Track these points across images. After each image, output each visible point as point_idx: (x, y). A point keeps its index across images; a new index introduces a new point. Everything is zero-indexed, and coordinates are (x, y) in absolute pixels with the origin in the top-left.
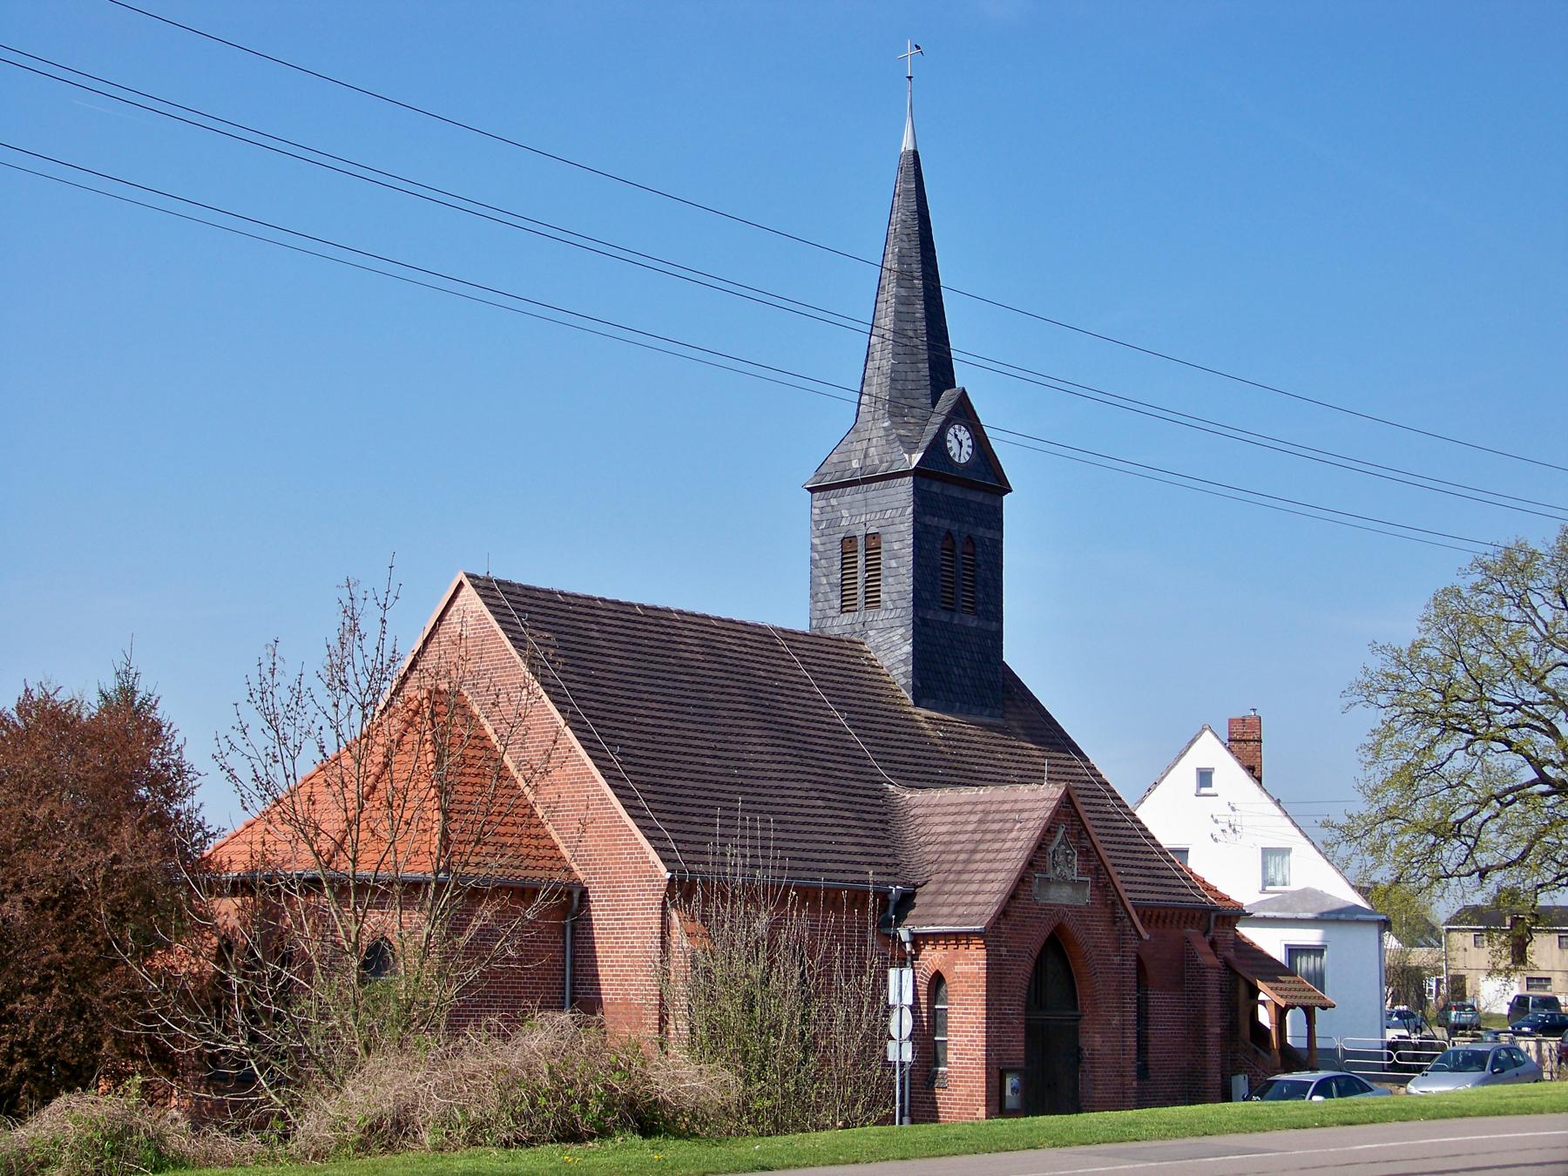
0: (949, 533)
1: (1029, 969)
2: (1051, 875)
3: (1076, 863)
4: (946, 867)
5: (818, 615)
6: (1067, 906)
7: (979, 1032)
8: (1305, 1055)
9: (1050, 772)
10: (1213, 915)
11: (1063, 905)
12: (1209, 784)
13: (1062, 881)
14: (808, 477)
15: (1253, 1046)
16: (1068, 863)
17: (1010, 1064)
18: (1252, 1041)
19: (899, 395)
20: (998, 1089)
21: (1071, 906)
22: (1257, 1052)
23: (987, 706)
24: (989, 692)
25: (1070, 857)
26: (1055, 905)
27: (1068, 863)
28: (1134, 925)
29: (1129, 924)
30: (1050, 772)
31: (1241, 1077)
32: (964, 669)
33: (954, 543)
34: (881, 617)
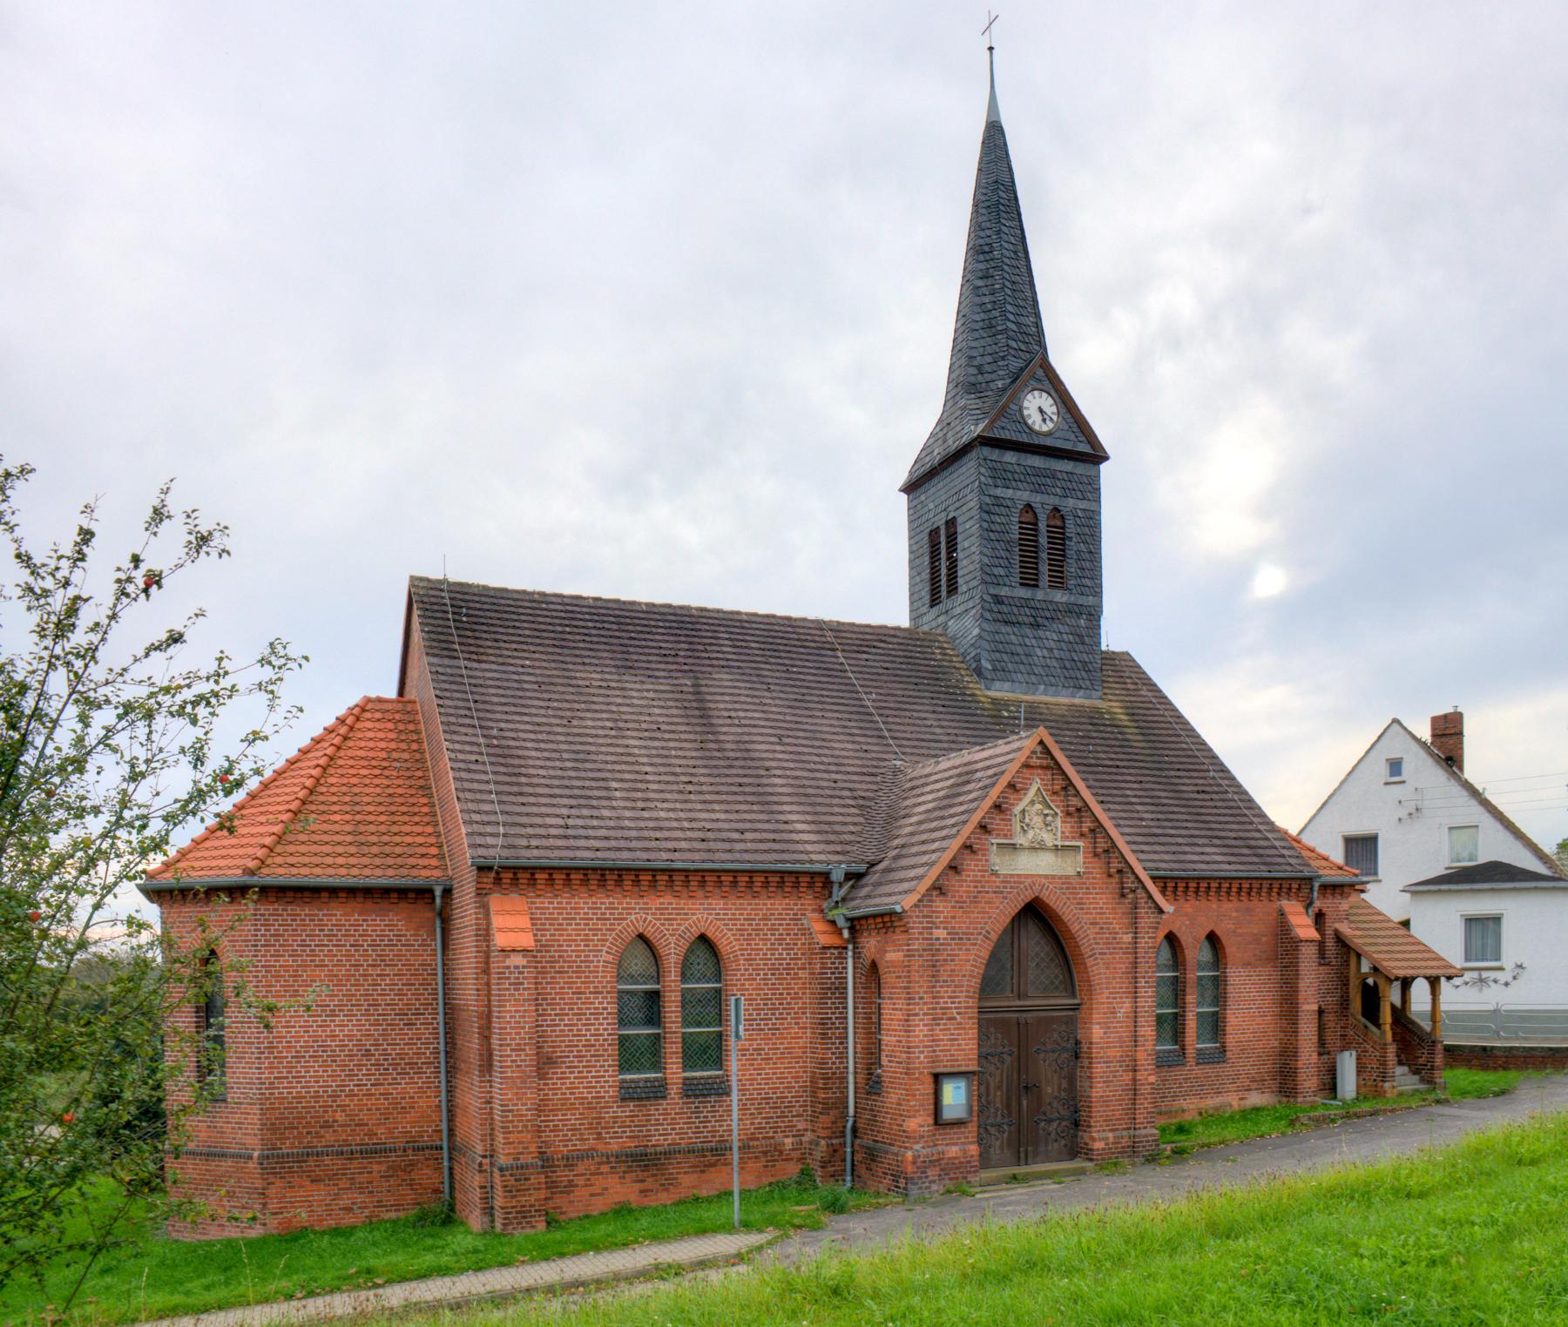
0: (1029, 507)
1: (985, 954)
2: (1020, 840)
3: (1059, 824)
4: (347, 799)
5: (915, 616)
6: (1046, 877)
7: (970, 1018)
8: (1426, 1025)
9: (1019, 719)
10: (1316, 885)
11: (1039, 876)
12: (1399, 773)
13: (1036, 847)
14: (902, 477)
15: (1363, 1020)
16: (1047, 825)
17: (952, 1066)
18: (1364, 1015)
19: (976, 372)
20: (932, 1097)
21: (1053, 877)
22: (1366, 1027)
23: (1081, 688)
24: (1083, 673)
25: (1049, 818)
26: (1027, 876)
27: (1047, 825)
28: (1150, 897)
29: (1144, 895)
30: (1019, 719)
31: (1347, 1054)
32: (1051, 650)
33: (1035, 513)
34: (958, 603)
